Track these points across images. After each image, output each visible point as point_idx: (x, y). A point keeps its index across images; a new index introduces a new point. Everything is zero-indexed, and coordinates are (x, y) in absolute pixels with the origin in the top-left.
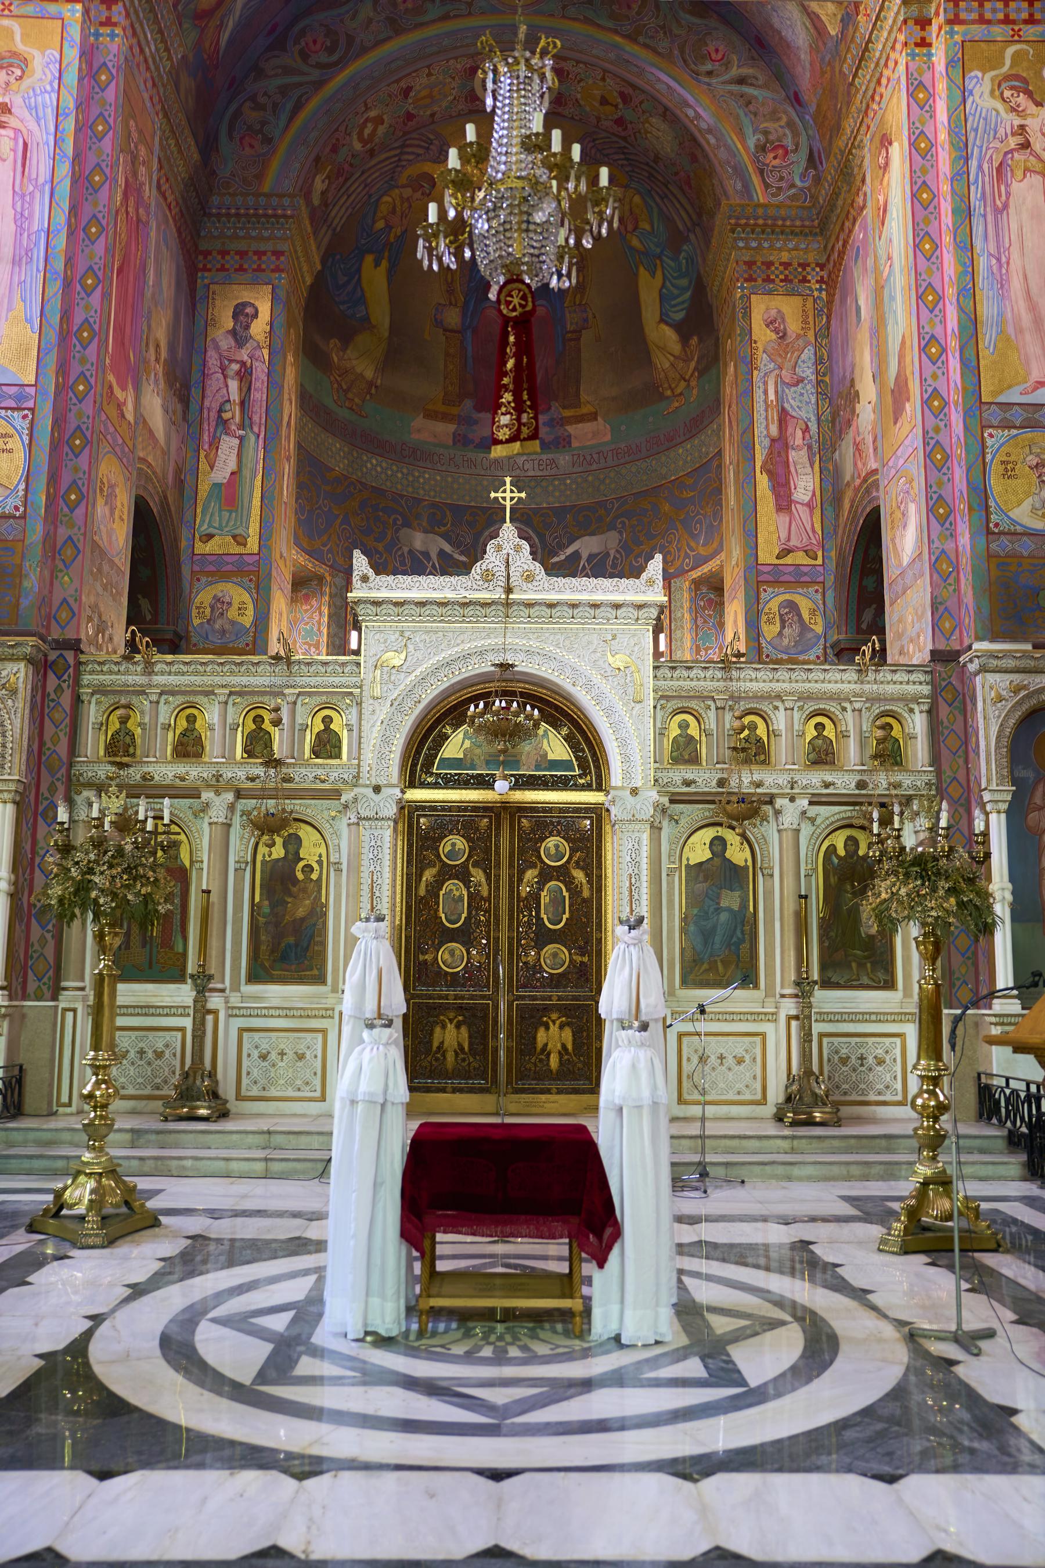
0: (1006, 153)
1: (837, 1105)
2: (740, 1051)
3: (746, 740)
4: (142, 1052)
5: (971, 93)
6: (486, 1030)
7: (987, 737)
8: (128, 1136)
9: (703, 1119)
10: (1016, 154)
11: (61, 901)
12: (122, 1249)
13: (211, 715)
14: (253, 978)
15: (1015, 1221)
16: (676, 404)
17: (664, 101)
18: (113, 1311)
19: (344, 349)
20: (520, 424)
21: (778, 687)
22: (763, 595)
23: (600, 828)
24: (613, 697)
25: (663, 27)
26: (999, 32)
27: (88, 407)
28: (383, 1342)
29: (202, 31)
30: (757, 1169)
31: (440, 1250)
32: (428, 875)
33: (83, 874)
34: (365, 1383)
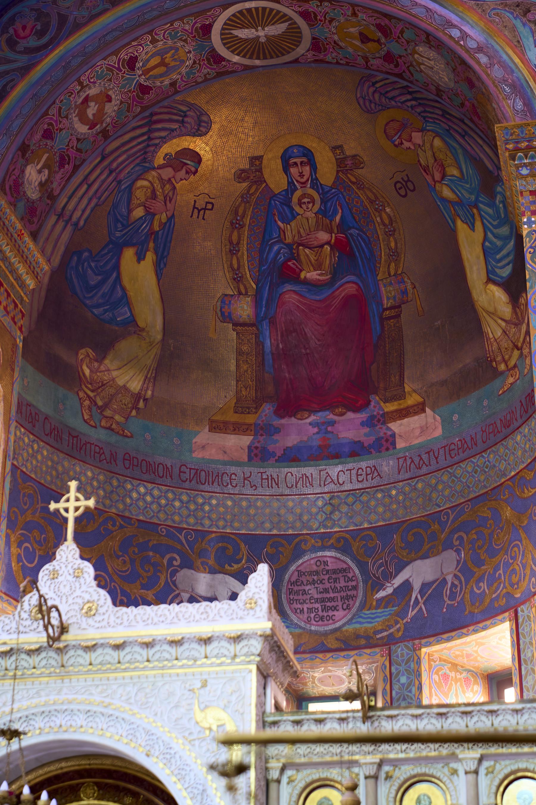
16: (511, 380)
17: (423, 25)
19: (101, 359)
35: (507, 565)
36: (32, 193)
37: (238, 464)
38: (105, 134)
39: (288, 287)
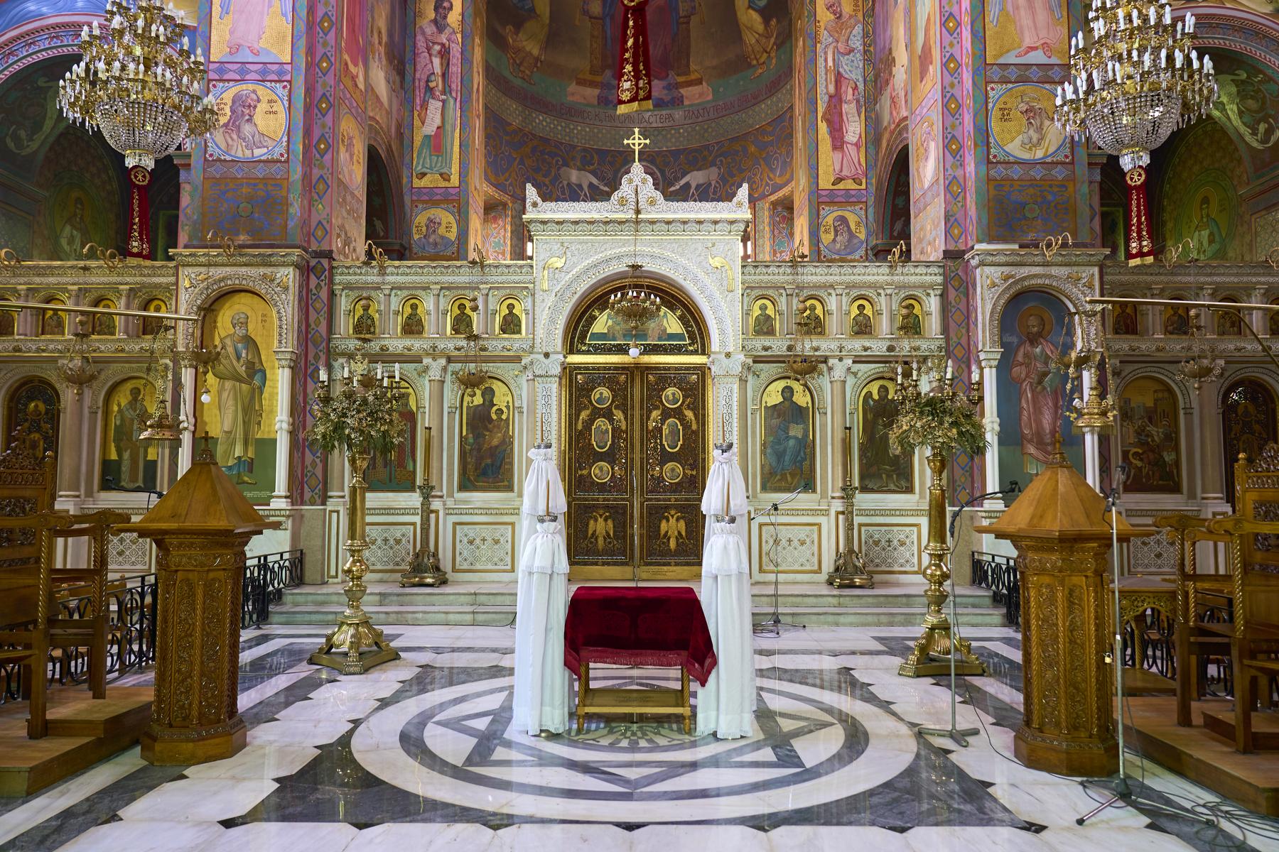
1: (871, 574)
2: (802, 536)
3: (808, 318)
4: (386, 540)
6: (625, 522)
7: (983, 313)
8: (377, 598)
9: (776, 583)
11: (324, 436)
12: (374, 675)
13: (428, 304)
14: (463, 487)
15: (997, 655)
18: (368, 717)
19: (517, 33)
20: (638, 88)
21: (831, 279)
22: (822, 212)
23: (704, 381)
24: (713, 288)
27: (330, 79)
28: (553, 737)
30: (814, 618)
31: (592, 674)
32: (584, 415)
33: (339, 417)
34: (541, 765)
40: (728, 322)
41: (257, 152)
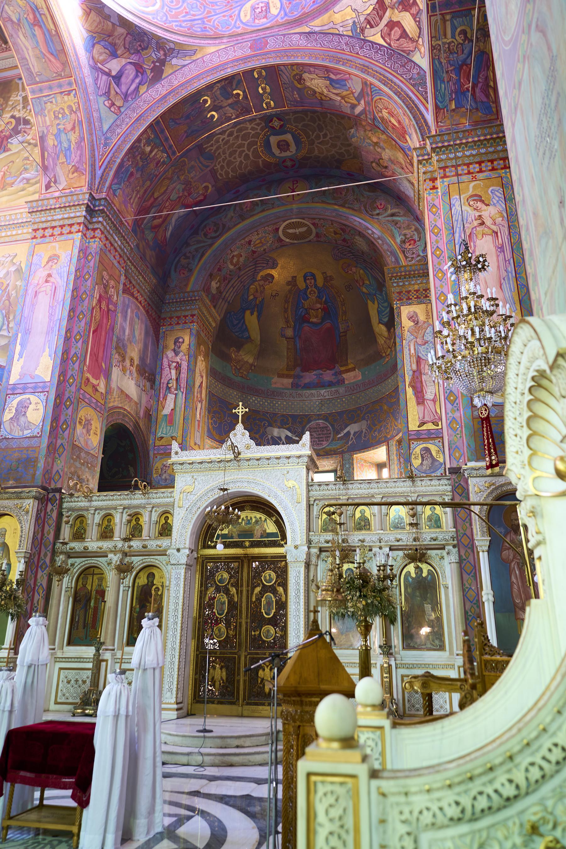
0: (473, 229)
4: (77, 681)
5: (454, 205)
10: (478, 228)
19: (238, 352)
22: (412, 446)
25: (356, 199)
26: (465, 178)
29: (156, 233)
32: (258, 590)
35: (385, 426)
36: (214, 291)
37: (288, 389)
38: (240, 269)
39: (305, 324)
40: (297, 524)
41: (26, 432)
